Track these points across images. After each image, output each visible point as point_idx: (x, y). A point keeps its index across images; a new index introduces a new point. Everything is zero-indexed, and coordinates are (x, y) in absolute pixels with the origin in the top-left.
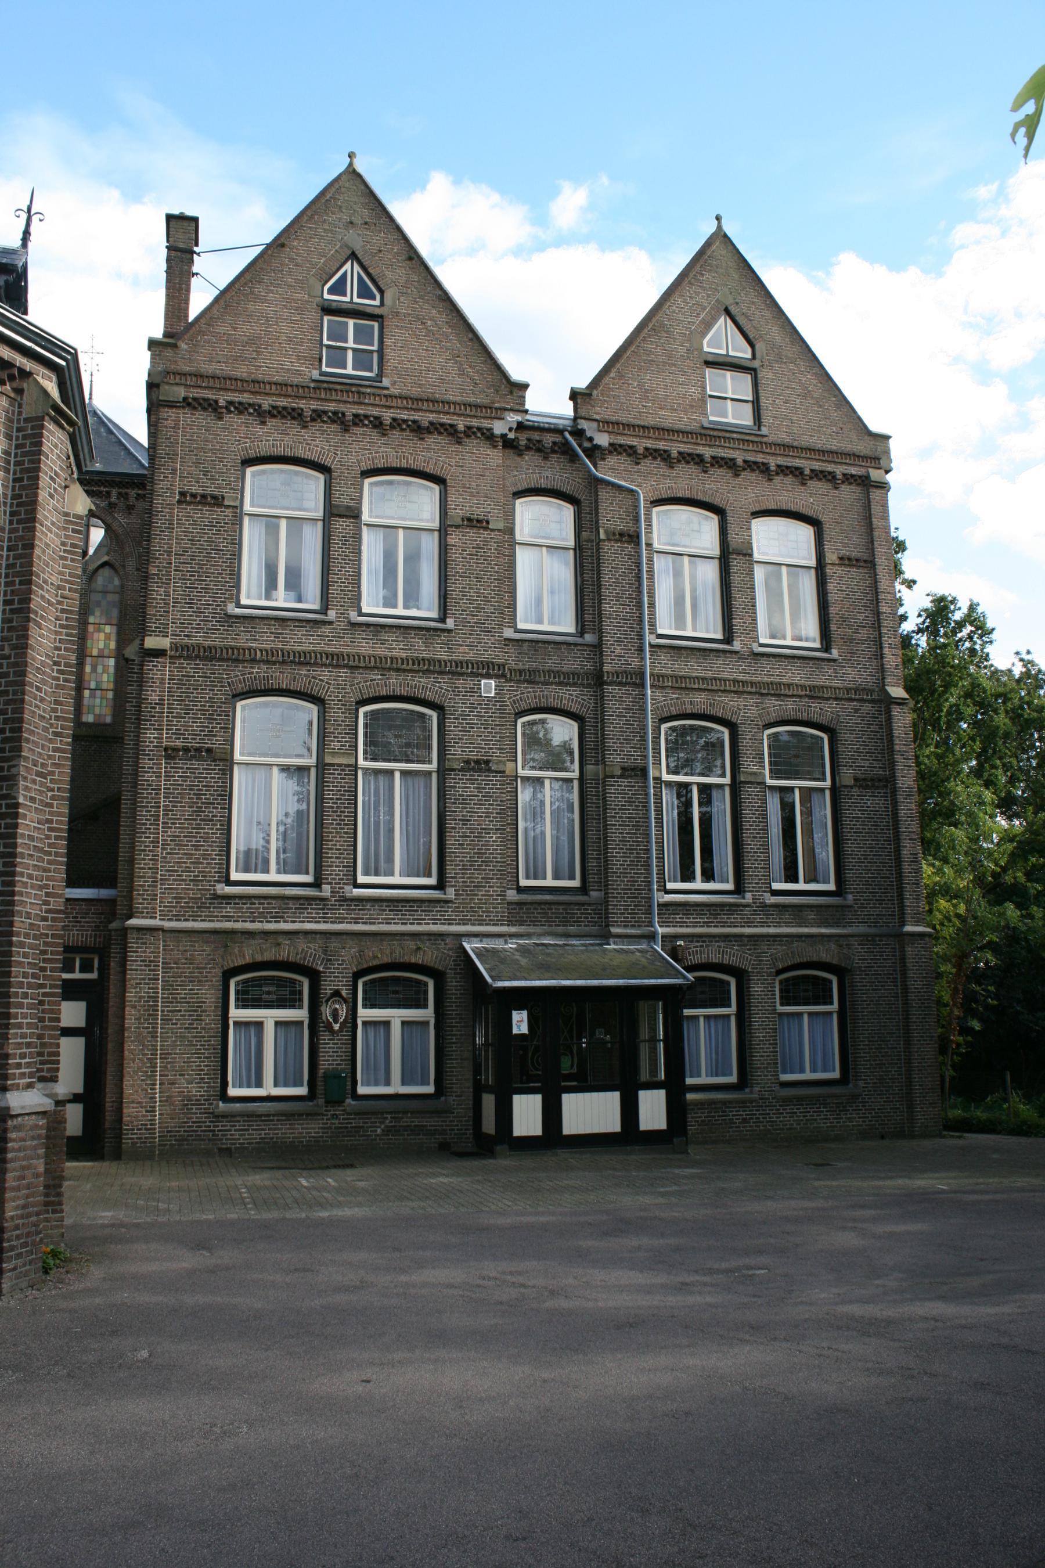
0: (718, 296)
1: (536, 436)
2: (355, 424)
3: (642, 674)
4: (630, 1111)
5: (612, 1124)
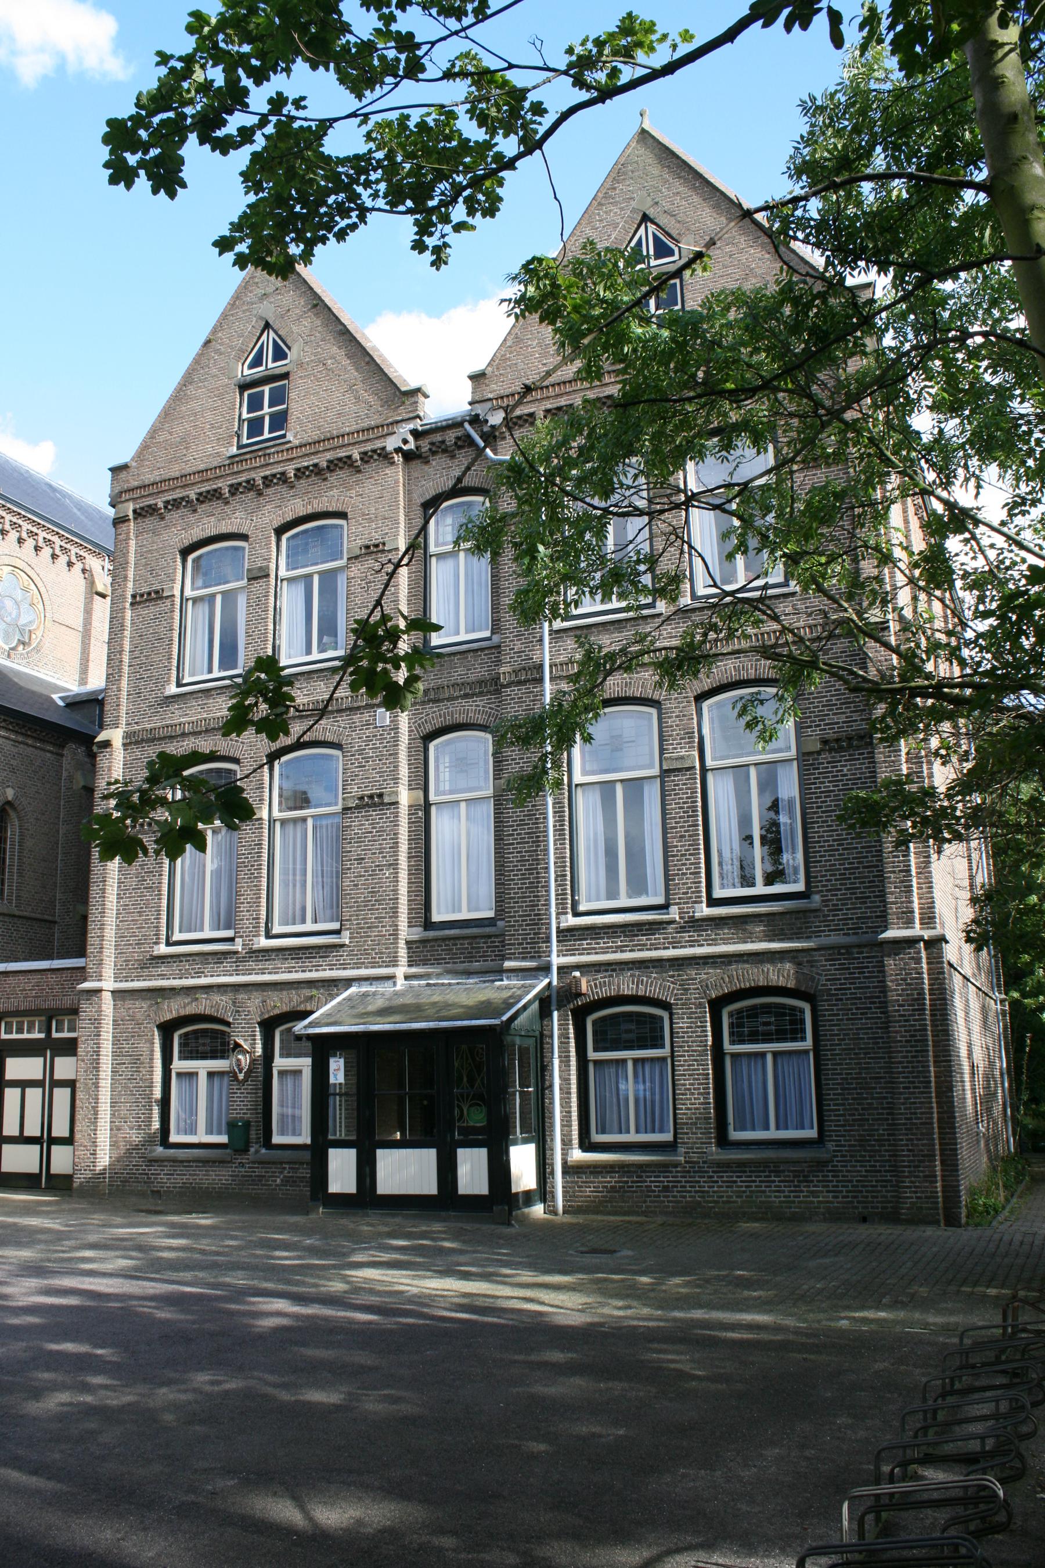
0: (633, 204)
1: (438, 437)
2: (267, 486)
3: (540, 667)
4: (447, 1170)
5: (429, 1186)
